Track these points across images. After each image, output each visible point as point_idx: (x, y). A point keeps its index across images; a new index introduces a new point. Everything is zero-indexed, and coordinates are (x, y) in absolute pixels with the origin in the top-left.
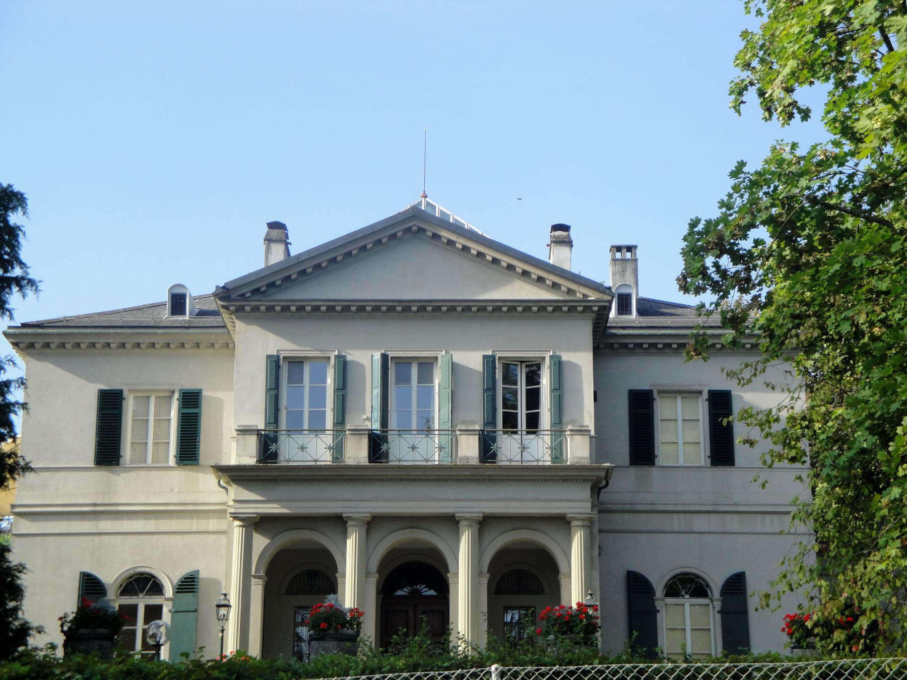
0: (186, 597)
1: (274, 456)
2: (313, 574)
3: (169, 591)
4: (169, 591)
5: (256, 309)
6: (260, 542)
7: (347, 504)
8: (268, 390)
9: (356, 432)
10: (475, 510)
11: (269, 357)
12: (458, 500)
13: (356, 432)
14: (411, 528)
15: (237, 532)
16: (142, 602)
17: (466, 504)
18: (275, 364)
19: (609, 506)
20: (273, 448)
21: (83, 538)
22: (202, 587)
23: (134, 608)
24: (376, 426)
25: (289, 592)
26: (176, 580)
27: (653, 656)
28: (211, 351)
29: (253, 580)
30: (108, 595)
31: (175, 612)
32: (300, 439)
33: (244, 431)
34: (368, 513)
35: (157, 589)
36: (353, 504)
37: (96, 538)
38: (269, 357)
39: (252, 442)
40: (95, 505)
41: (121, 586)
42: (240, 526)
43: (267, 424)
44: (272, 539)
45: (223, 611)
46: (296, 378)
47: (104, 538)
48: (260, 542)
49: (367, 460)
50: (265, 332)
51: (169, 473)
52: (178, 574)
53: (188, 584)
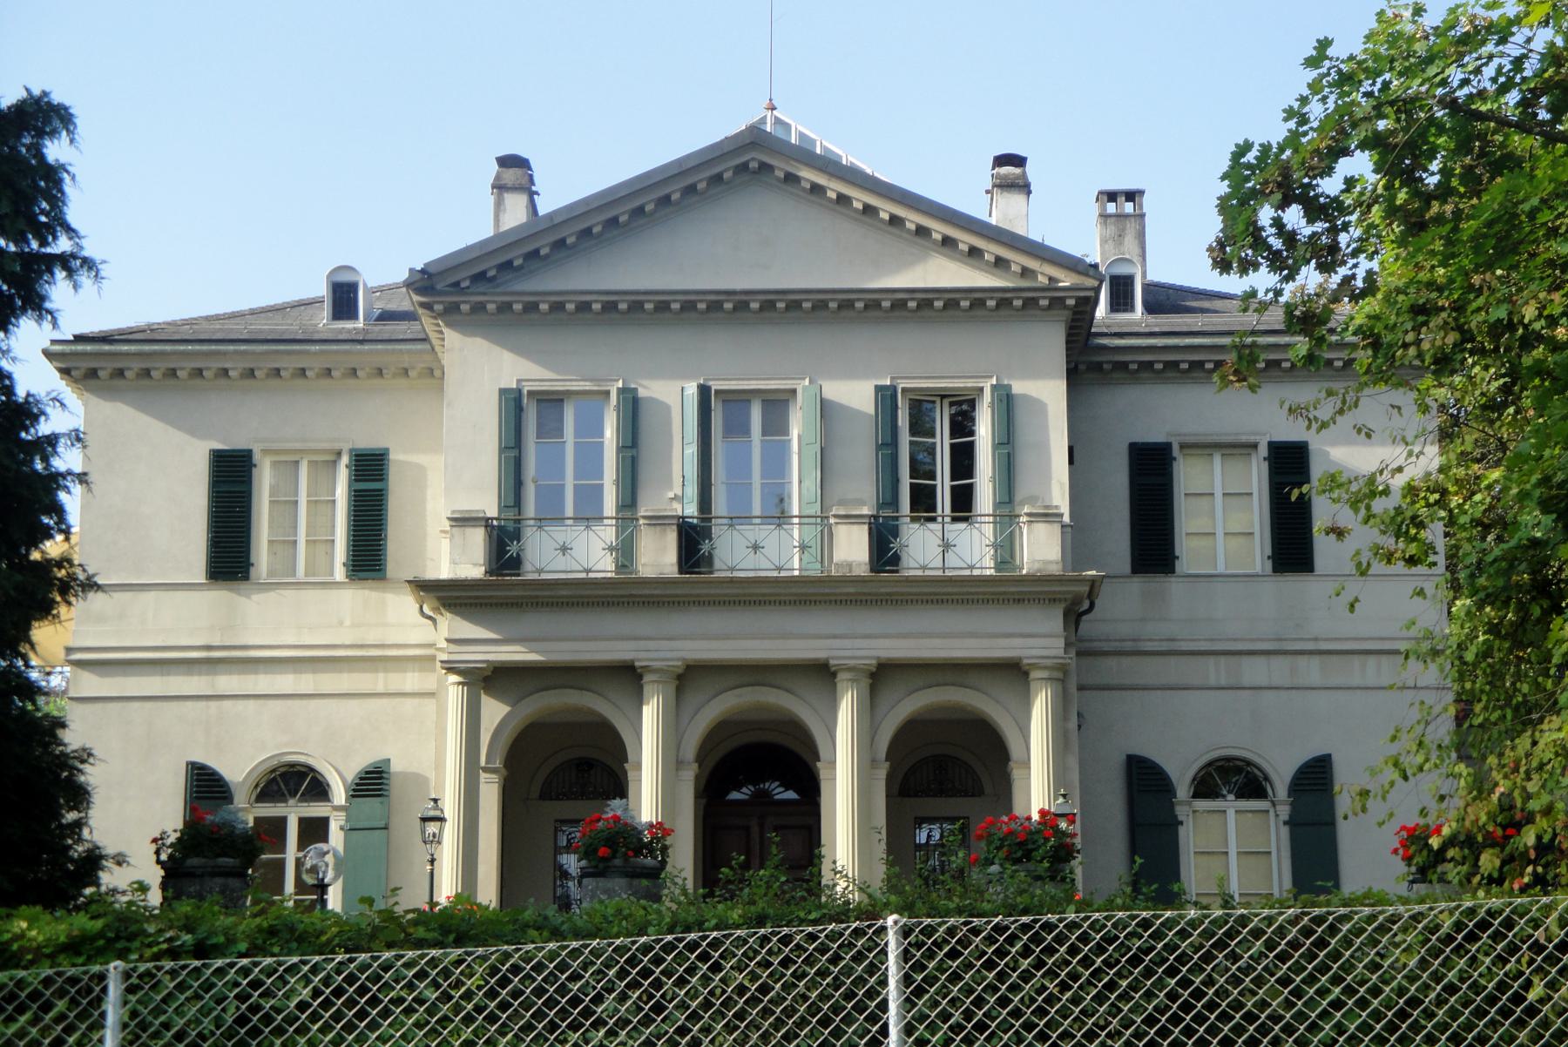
0: (370, 805)
1: (516, 563)
2: (585, 765)
3: (339, 795)
4: (339, 795)
5: (479, 308)
6: (494, 711)
7: (642, 644)
8: (502, 450)
9: (657, 521)
10: (669, 655)
11: (503, 392)
12: (835, 637)
13: (657, 521)
14: (752, 685)
15: (454, 693)
16: (293, 813)
17: (847, 643)
18: (513, 404)
19: (1096, 644)
20: (513, 549)
21: (189, 704)
22: (395, 788)
23: (282, 821)
24: (691, 510)
25: (545, 795)
26: (351, 776)
27: (1169, 898)
28: (403, 382)
29: (483, 776)
30: (236, 800)
31: (350, 830)
32: (560, 534)
33: (462, 521)
34: (678, 660)
35: (319, 790)
36: (651, 644)
37: (213, 704)
38: (503, 392)
39: (478, 537)
40: (209, 648)
41: (257, 786)
42: (459, 683)
43: (502, 508)
44: (513, 705)
45: (432, 828)
46: (551, 428)
47: (227, 704)
48: (494, 711)
49: (676, 569)
50: (496, 350)
51: (334, 594)
52: (353, 769)
53: (372, 783)
